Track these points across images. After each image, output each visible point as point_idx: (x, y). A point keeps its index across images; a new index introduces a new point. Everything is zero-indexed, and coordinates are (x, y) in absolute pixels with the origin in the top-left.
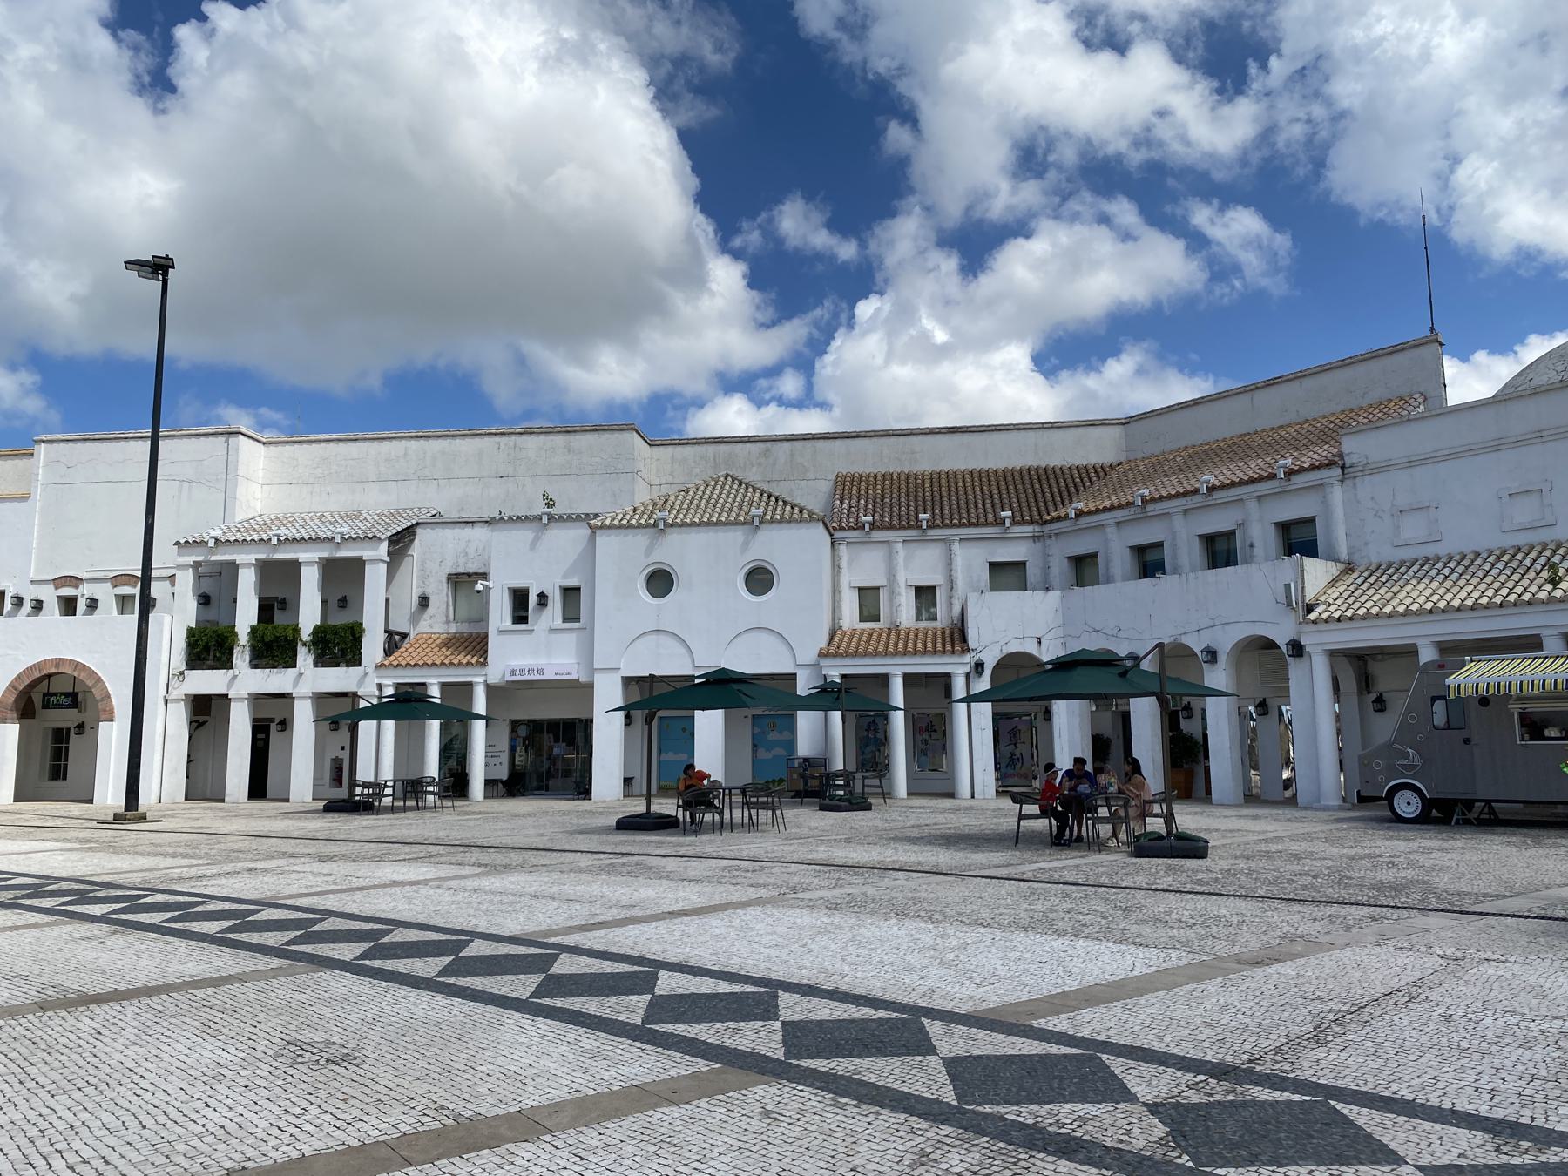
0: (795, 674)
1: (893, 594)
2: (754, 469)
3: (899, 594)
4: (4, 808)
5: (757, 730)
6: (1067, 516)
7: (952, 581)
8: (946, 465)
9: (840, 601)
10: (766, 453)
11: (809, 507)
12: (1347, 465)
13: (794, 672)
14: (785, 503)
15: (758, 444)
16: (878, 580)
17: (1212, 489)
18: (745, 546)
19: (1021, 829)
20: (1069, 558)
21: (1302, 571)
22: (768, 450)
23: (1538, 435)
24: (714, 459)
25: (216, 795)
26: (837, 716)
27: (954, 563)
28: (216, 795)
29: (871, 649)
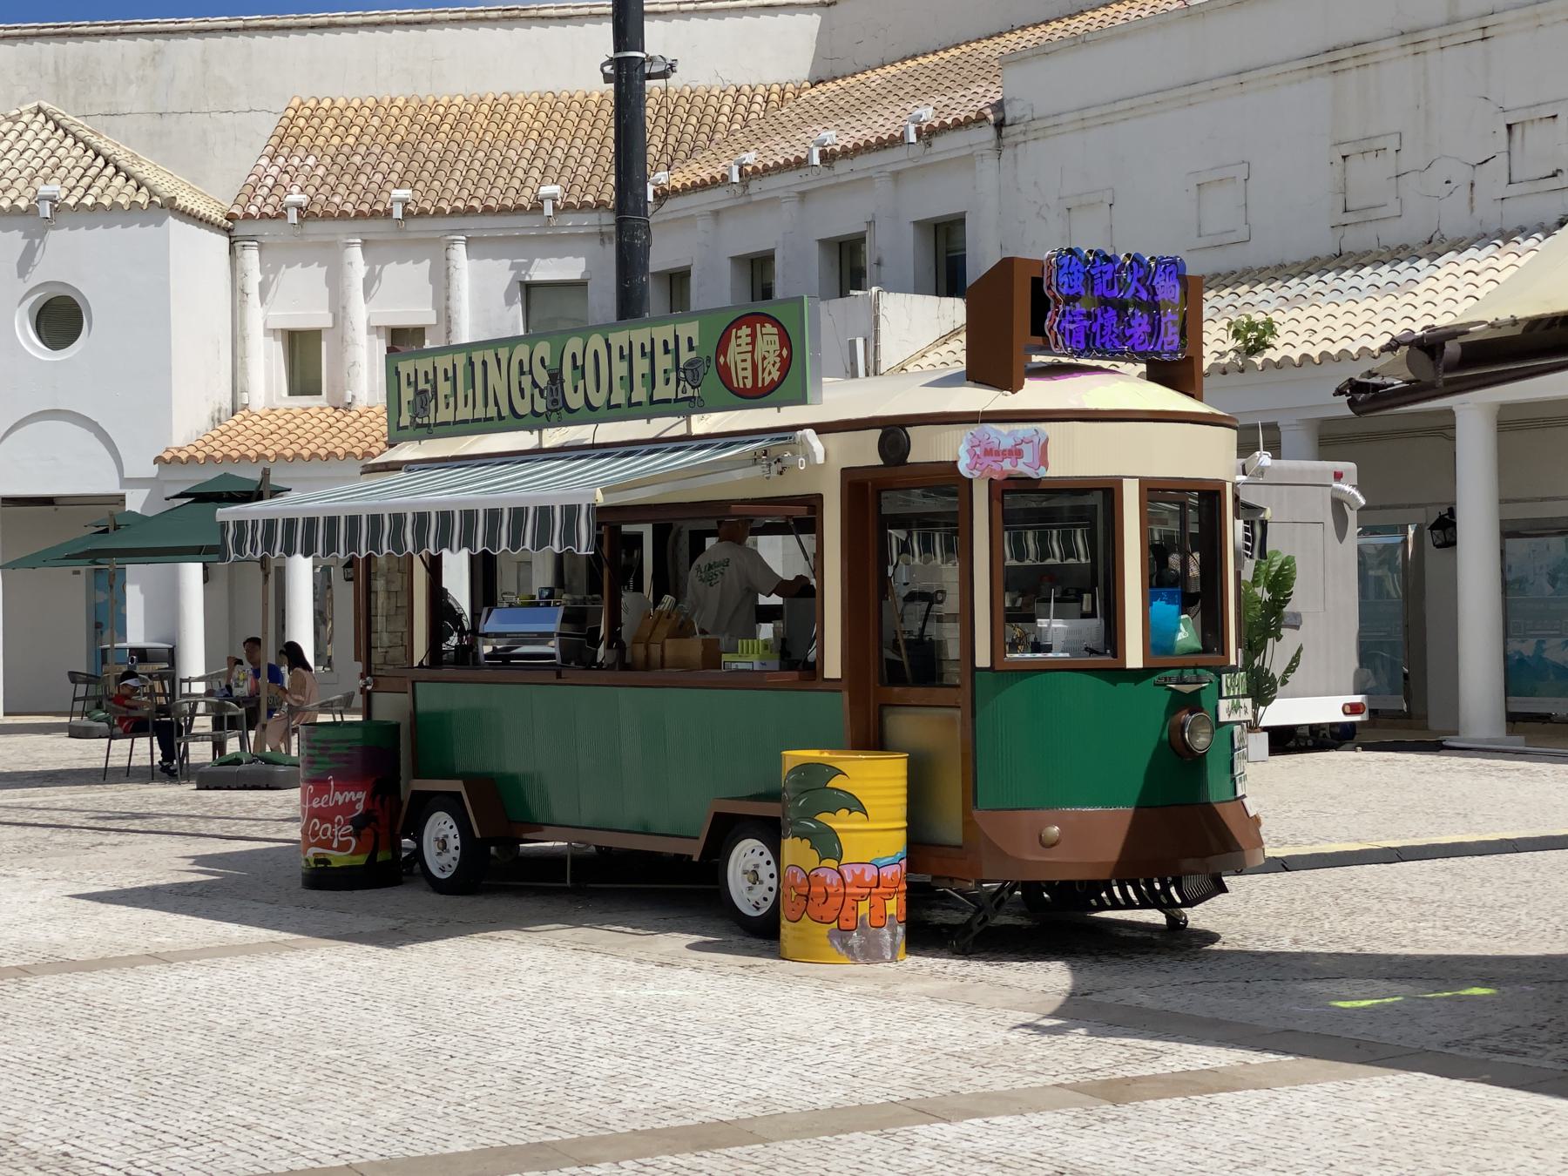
0: (124, 496)
1: (342, 342)
2: (133, 89)
3: (354, 343)
4: (1566, 759)
5: (102, 597)
6: (388, 213)
7: (449, 319)
8: (494, 87)
9: (244, 357)
10: (155, 58)
11: (151, 182)
12: (1008, 121)
13: (121, 492)
14: (118, 169)
15: (141, 41)
16: (314, 316)
17: (828, 157)
18: (25, 264)
19: (132, 764)
20: (732, 258)
21: (877, 319)
22: (159, 52)
23: (1192, 100)
24: (56, 69)
25: (253, 521)
26: (192, 572)
27: (454, 283)
28: (253, 521)
29: (640, 394)
